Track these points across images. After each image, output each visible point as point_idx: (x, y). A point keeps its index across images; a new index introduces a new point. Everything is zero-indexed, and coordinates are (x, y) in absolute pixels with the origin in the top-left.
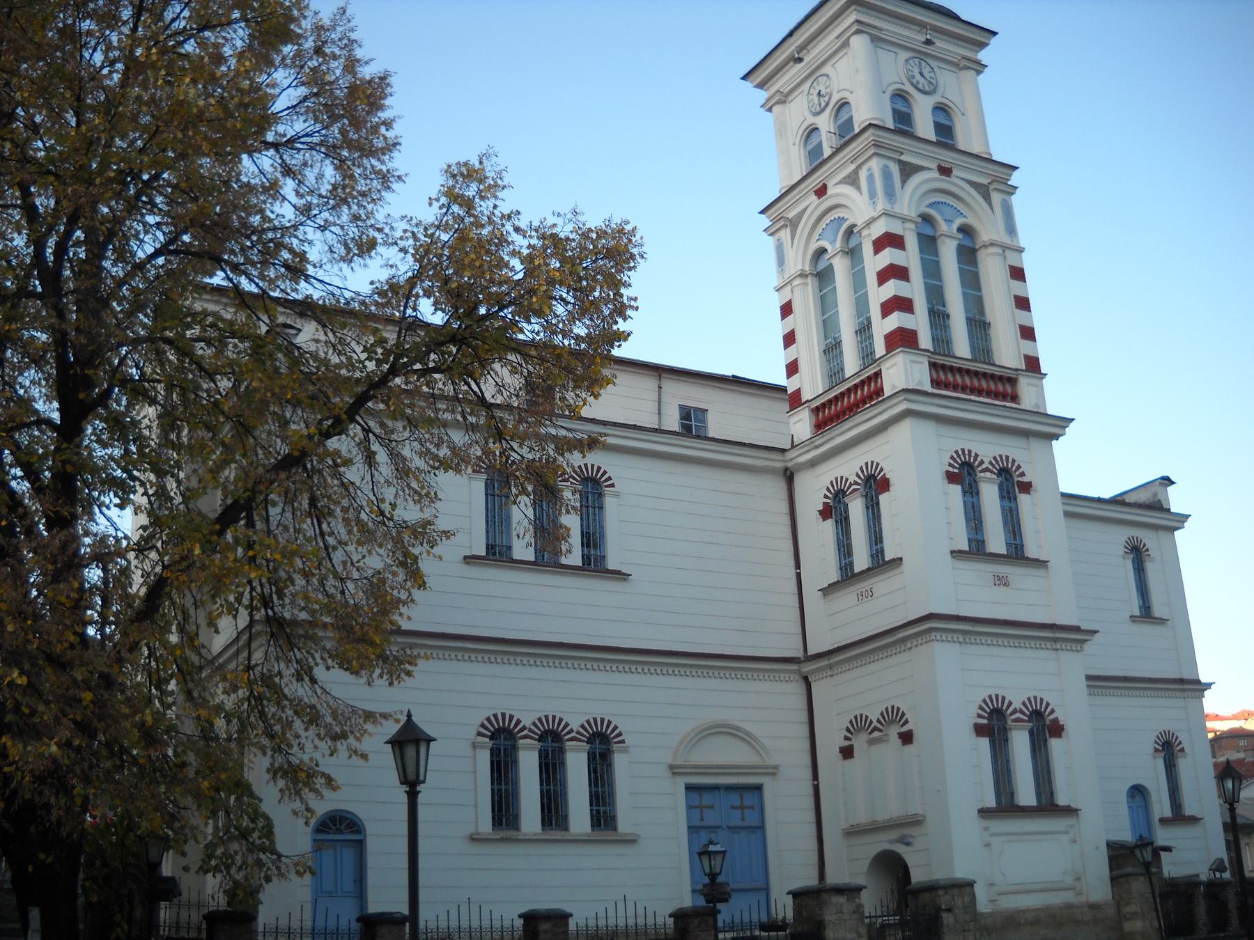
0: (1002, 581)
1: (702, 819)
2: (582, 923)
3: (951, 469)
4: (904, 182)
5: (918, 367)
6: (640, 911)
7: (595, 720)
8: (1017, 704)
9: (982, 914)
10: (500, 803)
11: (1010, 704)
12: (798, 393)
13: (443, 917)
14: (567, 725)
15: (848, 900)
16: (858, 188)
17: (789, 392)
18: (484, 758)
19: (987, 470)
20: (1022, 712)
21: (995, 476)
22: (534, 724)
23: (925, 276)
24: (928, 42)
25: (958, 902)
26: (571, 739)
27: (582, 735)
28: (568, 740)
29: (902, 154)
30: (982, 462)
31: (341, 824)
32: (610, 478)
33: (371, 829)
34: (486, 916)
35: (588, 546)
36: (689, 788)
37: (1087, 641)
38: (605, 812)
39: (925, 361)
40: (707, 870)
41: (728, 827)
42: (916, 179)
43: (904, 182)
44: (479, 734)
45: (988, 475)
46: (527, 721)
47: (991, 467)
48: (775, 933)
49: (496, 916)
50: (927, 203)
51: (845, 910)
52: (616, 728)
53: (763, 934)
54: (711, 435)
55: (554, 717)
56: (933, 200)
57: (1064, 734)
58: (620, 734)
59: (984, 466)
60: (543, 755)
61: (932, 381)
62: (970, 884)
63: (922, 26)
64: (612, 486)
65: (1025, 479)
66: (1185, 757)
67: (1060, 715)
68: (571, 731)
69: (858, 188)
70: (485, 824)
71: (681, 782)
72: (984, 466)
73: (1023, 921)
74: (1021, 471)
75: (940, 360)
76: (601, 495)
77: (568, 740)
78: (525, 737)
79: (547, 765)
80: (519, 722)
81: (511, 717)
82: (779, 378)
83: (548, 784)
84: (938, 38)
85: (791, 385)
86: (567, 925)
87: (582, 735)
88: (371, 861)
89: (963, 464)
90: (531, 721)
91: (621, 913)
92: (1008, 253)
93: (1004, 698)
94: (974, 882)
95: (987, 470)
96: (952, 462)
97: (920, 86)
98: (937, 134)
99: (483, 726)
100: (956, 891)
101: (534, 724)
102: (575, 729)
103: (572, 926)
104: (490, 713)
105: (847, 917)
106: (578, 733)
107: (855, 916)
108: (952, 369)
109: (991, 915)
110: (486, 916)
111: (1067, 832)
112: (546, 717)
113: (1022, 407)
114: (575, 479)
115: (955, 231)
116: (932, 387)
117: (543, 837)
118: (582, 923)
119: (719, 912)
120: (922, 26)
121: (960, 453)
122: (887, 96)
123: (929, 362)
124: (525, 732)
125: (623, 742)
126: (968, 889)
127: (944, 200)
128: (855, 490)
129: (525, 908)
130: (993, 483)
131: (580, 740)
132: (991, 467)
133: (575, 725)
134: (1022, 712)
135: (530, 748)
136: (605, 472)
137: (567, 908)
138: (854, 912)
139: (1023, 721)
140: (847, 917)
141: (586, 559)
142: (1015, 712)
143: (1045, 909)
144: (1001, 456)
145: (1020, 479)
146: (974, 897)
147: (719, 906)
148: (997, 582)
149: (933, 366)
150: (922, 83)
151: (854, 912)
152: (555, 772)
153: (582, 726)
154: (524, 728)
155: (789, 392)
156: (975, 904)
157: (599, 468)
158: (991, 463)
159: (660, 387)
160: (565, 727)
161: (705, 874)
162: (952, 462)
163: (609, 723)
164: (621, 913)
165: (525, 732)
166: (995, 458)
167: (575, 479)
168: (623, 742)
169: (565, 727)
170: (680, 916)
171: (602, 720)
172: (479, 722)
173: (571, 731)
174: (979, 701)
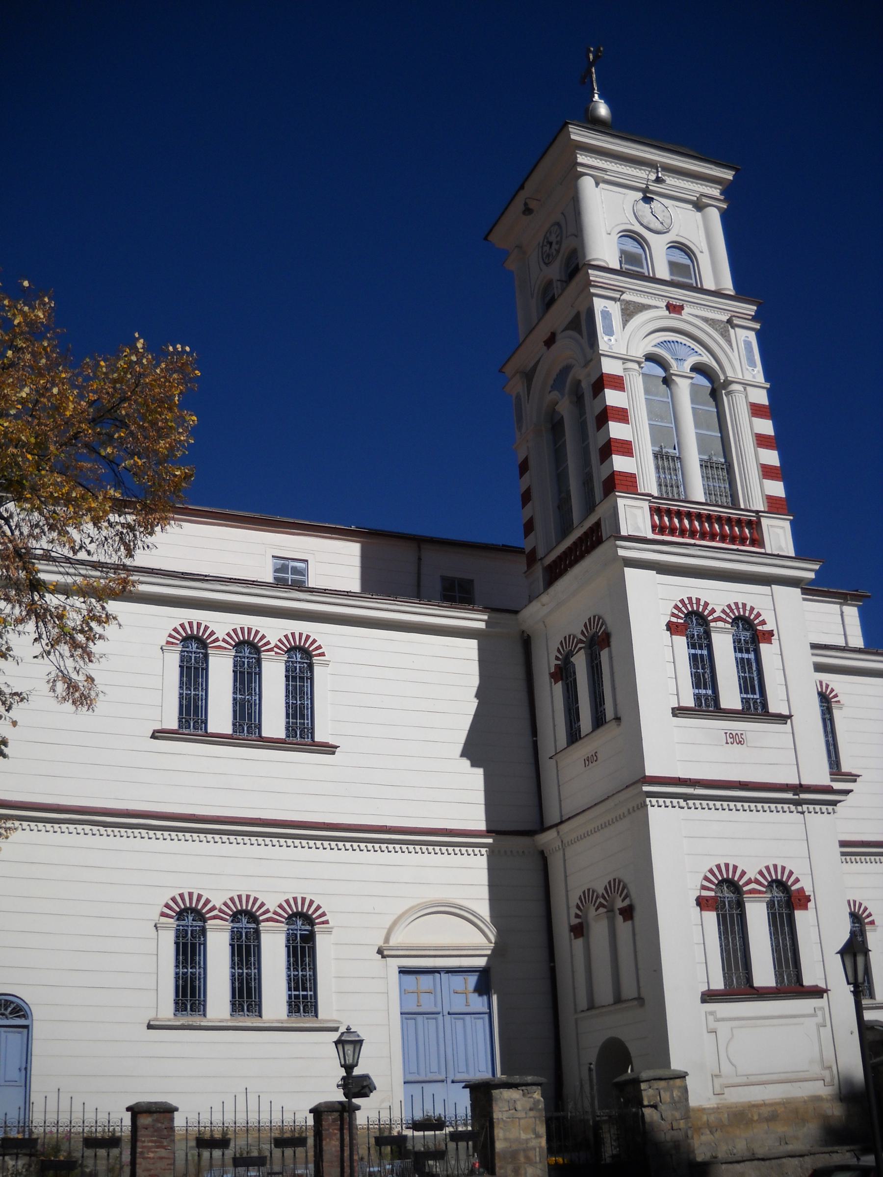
0: (737, 739)
1: (467, 1005)
2: (374, 1116)
3: (674, 620)
4: (625, 322)
5: (638, 512)
6: (65, 1105)
7: (295, 899)
8: (751, 874)
9: (702, 1110)
10: (241, 989)
11: (743, 873)
12: (534, 551)
13: (217, 1108)
14: (208, 901)
15: (524, 1095)
16: (580, 332)
17: (526, 553)
18: (168, 939)
19: (719, 619)
20: (757, 882)
21: (729, 626)
22: (225, 904)
23: (650, 419)
24: (658, 180)
25: (666, 1096)
26: (268, 920)
27: (280, 915)
28: (264, 921)
29: (623, 293)
30: (713, 611)
31: (6, 1009)
32: (319, 647)
33: (38, 1013)
34: (265, 1107)
35: (295, 717)
36: (404, 971)
37: (840, 801)
38: (305, 997)
39: (646, 505)
40: (343, 1063)
41: (449, 1014)
42: (640, 318)
43: (625, 322)
44: (163, 915)
45: (720, 624)
46: (217, 901)
47: (724, 616)
48: (433, 1133)
49: (90, 1108)
50: (654, 343)
51: (519, 1107)
52: (318, 908)
53: (416, 1133)
54: (311, 584)
55: (248, 897)
56: (662, 339)
57: (811, 905)
58: (323, 914)
59: (715, 615)
60: (291, 939)
61: (654, 527)
62: (682, 1076)
63: (651, 165)
64: (322, 654)
65: (766, 628)
66: (875, 930)
67: (805, 884)
68: (267, 911)
69: (580, 332)
70: (166, 1010)
71: (394, 964)
72: (715, 615)
73: (756, 1118)
74: (761, 619)
75: (664, 504)
76: (311, 667)
77: (264, 921)
78: (215, 917)
79: (240, 947)
80: (208, 901)
81: (200, 897)
82: (516, 539)
83: (296, 969)
84: (669, 176)
85: (527, 545)
86: (172, 1120)
87: (280, 915)
88: (37, 1048)
89: (689, 615)
90: (223, 901)
91: (241, 1106)
92: (749, 389)
93: (783, 868)
94: (686, 1074)
95: (719, 619)
96: (676, 612)
97: (652, 226)
98: (672, 273)
99: (167, 906)
100: (662, 1084)
101: (225, 904)
102: (218, 906)
103: (179, 1120)
104: (175, 893)
105: (521, 1114)
106: (275, 913)
107: (532, 1114)
108: (679, 514)
109: (717, 1110)
110: (265, 1107)
111: (814, 1015)
112: (240, 897)
113: (769, 551)
114: (280, 648)
115: (688, 371)
116: (653, 531)
117: (229, 1024)
118: (193, 1119)
119: (358, 1108)
120: (651, 165)
121: (734, 607)
122: (615, 237)
123: (650, 508)
124: (215, 912)
125: (327, 922)
126: (678, 1082)
127: (674, 339)
128: (580, 649)
129: (131, 1102)
130: (729, 633)
131: (277, 921)
132: (724, 616)
133: (272, 904)
134: (757, 882)
135: (221, 929)
136: (314, 641)
137: (172, 1101)
138: (531, 1109)
139: (760, 892)
140: (521, 1114)
141: (183, 721)
142: (749, 882)
143: (786, 1103)
144: (736, 604)
145: (759, 628)
146: (685, 1090)
147: (356, 1101)
148: (729, 740)
149: (656, 511)
150: (655, 225)
151: (531, 1109)
152: (193, 954)
153: (281, 906)
154: (213, 908)
155: (526, 553)
156: (687, 1099)
157: (308, 637)
158: (724, 611)
159: (420, 559)
160: (320, 916)
161: (342, 1066)
162: (676, 612)
163: (312, 902)
164: (241, 1106)
165: (215, 912)
166: (729, 606)
167: (280, 648)
168: (327, 922)
169: (320, 916)
170: (318, 1112)
171: (303, 899)
172: (164, 903)
173: (267, 911)
174: (704, 870)
